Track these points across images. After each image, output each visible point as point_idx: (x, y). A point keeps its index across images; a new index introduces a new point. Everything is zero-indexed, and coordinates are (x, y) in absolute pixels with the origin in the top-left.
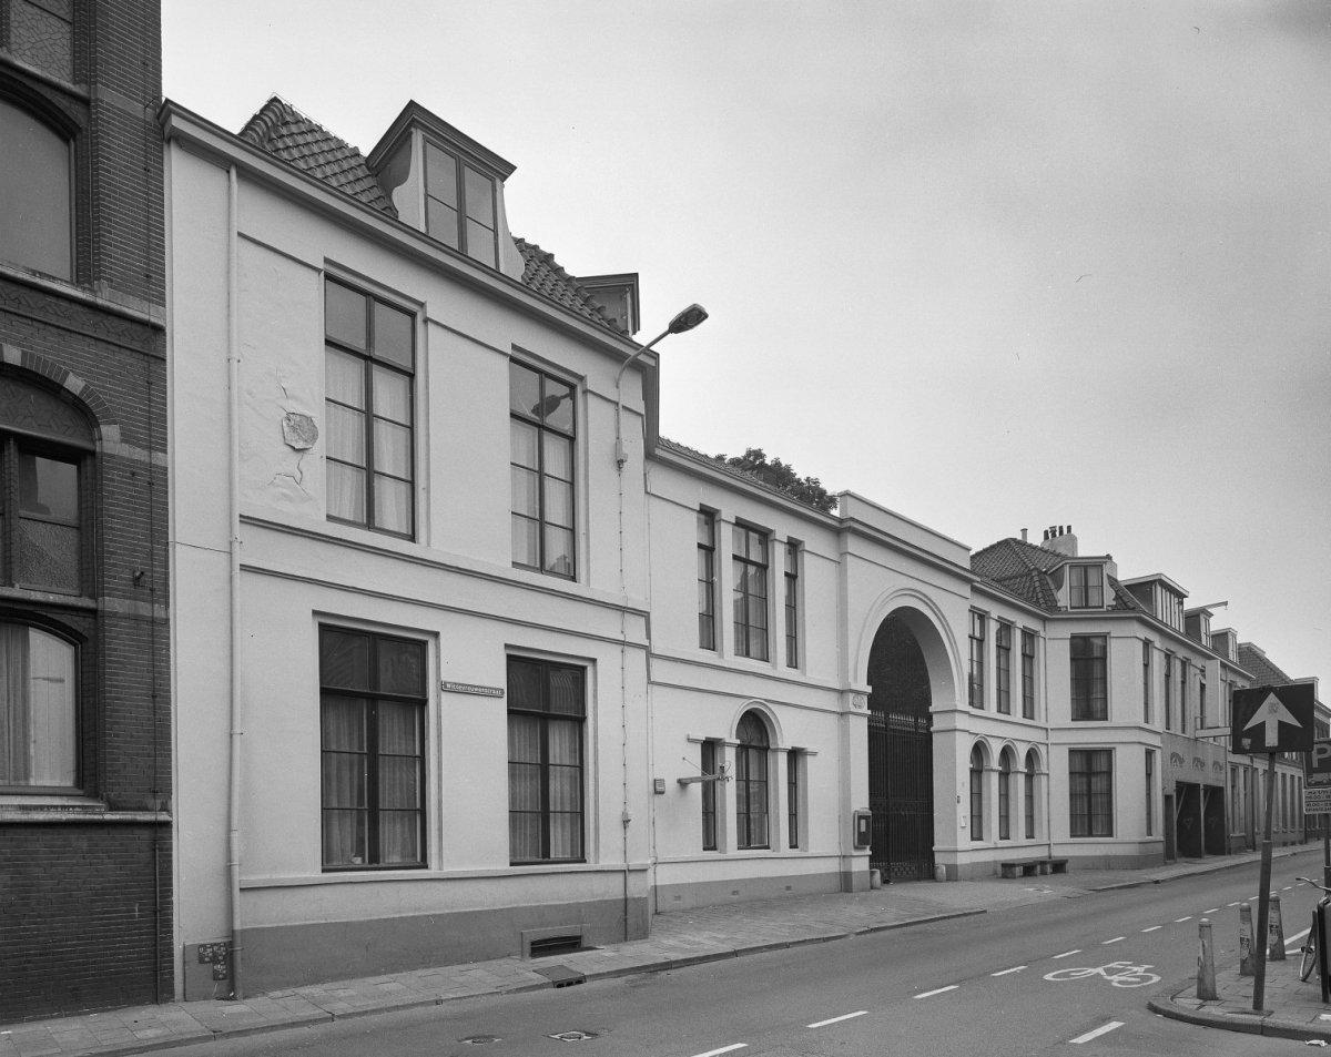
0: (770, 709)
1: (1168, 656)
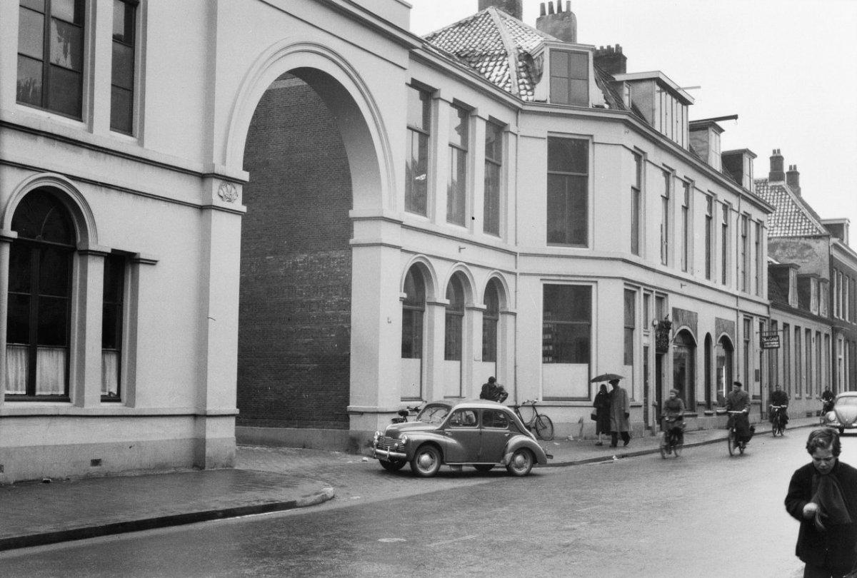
0: (430, 263)
1: (710, 198)
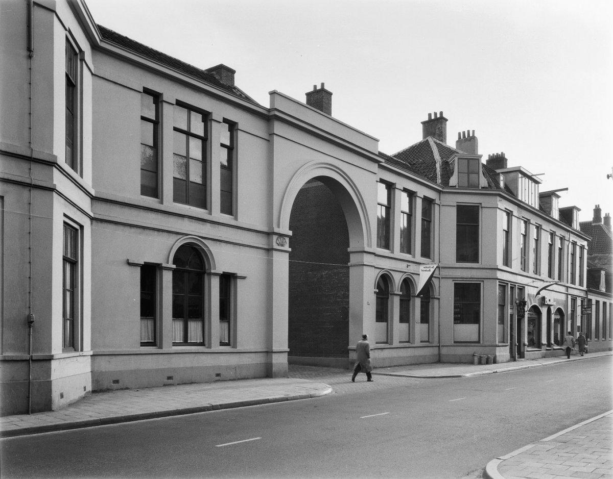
1: (553, 235)
